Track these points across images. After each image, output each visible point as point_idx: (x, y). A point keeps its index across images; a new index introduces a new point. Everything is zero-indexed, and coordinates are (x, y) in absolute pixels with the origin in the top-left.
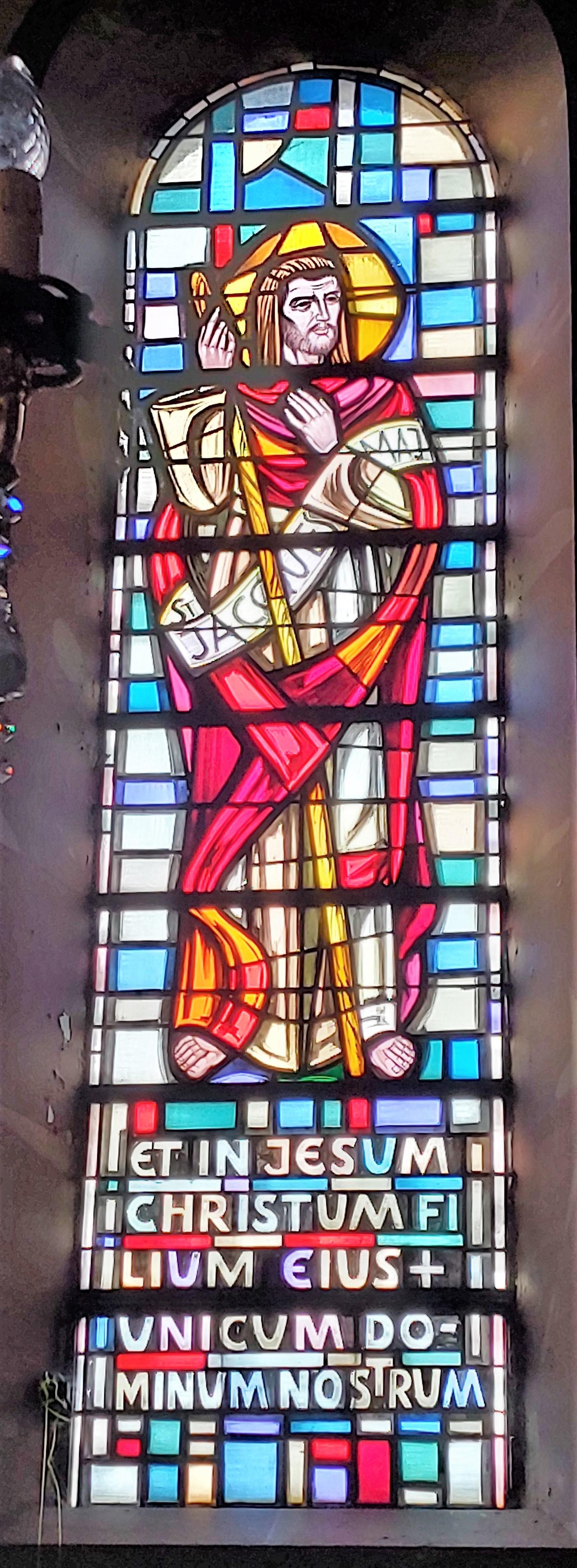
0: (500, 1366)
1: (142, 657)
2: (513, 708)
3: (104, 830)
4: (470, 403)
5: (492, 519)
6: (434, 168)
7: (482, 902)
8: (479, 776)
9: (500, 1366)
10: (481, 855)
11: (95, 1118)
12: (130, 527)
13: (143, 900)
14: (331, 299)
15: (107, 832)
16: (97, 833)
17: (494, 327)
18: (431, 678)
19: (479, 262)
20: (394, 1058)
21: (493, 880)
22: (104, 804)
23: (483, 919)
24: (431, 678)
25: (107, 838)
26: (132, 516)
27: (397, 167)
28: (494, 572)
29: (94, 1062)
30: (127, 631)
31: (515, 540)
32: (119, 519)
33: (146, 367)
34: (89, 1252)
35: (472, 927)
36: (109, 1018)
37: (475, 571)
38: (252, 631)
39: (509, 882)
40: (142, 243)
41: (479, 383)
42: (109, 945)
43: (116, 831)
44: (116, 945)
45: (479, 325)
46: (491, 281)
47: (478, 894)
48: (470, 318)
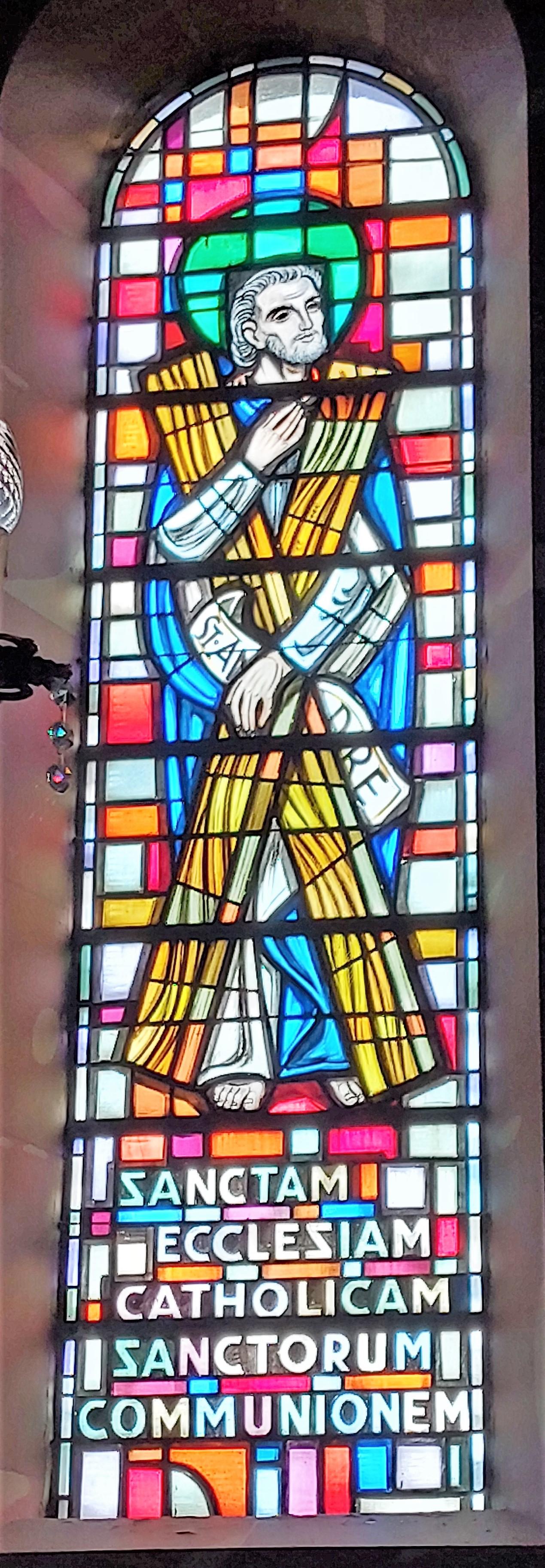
3: (69, 1284)
4: (452, 832)
5: (469, 539)
8: (458, 592)
11: (91, 773)
14: (311, 306)
15: (89, 870)
16: (77, 869)
17: (471, 340)
19: (460, 623)
22: (60, 1494)
25: (88, 877)
29: (69, 1350)
32: (71, 1241)
33: (84, 1515)
34: (92, 845)
36: (106, 611)
37: (455, 591)
41: (461, 939)
43: (98, 868)
48: (448, 511)
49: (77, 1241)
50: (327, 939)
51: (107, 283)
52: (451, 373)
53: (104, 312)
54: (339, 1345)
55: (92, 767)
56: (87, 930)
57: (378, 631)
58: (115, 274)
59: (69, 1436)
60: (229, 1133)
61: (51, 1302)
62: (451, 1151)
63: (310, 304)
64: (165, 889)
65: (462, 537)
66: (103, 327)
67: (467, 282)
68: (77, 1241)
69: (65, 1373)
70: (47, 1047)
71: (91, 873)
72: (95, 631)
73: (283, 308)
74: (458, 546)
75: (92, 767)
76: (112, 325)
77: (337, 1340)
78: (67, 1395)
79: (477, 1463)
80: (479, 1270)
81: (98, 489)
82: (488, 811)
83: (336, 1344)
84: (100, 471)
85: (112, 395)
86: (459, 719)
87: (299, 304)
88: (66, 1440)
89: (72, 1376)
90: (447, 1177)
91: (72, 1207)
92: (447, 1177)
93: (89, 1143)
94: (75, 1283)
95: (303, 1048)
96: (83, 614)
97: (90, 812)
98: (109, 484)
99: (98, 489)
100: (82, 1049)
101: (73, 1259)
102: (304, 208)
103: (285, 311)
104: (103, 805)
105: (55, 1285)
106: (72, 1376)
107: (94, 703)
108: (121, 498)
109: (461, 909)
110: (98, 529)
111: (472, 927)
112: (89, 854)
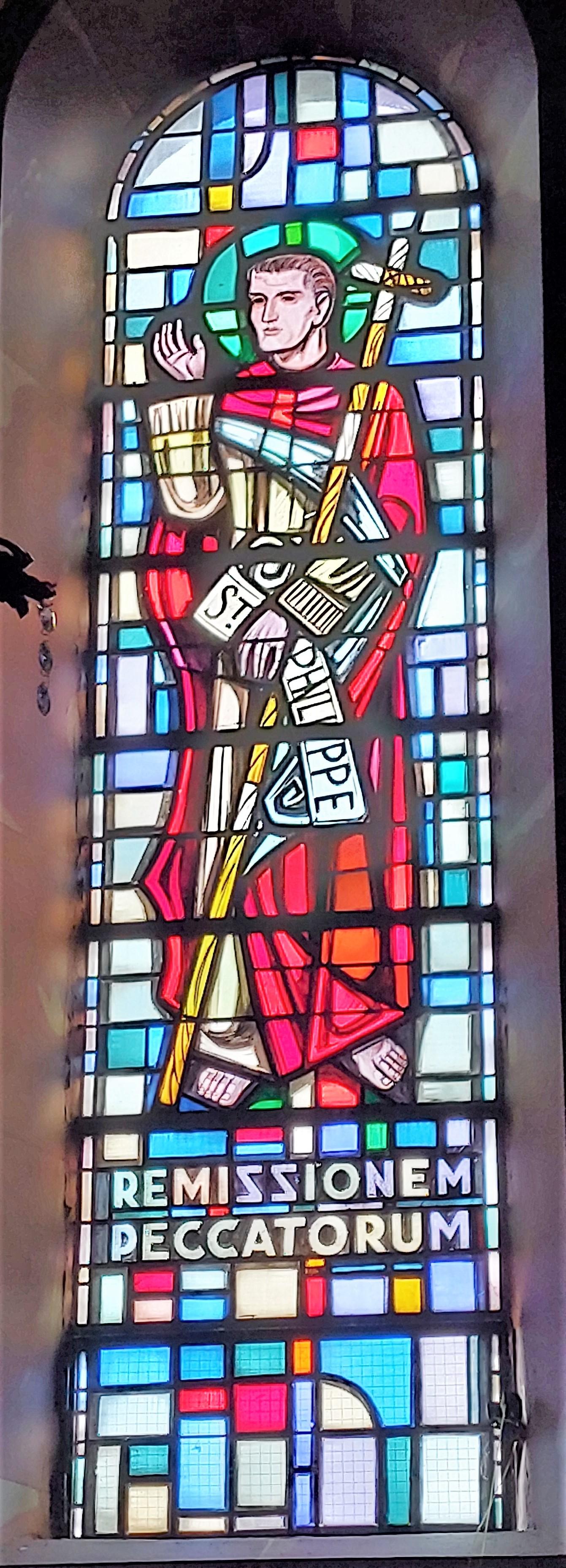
0: (467, 154)
1: (134, 501)
2: (498, 616)
6: (413, 166)
7: (474, 922)
9: (467, 154)
10: (474, 973)
12: (116, 541)
13: (130, 930)
18: (425, 976)
20: (391, 1062)
21: (486, 899)
23: (471, 742)
24: (425, 976)
26: (117, 525)
27: (375, 166)
28: (494, 1078)
30: (119, 481)
31: (517, 1116)
35: (462, 751)
38: (238, 540)
39: (502, 903)
40: (122, 285)
41: (471, 742)
42: (103, 888)
44: (111, 791)
45: (456, 159)
46: (479, 451)
47: (469, 913)
51: (105, 628)
52: (468, 718)
53: (102, 645)
56: (88, 1118)
59: (83, 1227)
61: (83, 541)
62: (461, 653)
65: (467, 184)
70: (64, 771)
72: (88, 1153)
74: (463, 192)
76: (100, 1079)
79: (487, 946)
80: (496, 1202)
82: (502, 855)
84: (108, 460)
86: (462, 186)
90: (454, 678)
92: (454, 678)
93: (114, 580)
100: (101, 714)
104: (103, 1029)
105: (89, 449)
108: (124, 663)
109: (482, 1308)
110: (96, 883)
111: (483, 728)
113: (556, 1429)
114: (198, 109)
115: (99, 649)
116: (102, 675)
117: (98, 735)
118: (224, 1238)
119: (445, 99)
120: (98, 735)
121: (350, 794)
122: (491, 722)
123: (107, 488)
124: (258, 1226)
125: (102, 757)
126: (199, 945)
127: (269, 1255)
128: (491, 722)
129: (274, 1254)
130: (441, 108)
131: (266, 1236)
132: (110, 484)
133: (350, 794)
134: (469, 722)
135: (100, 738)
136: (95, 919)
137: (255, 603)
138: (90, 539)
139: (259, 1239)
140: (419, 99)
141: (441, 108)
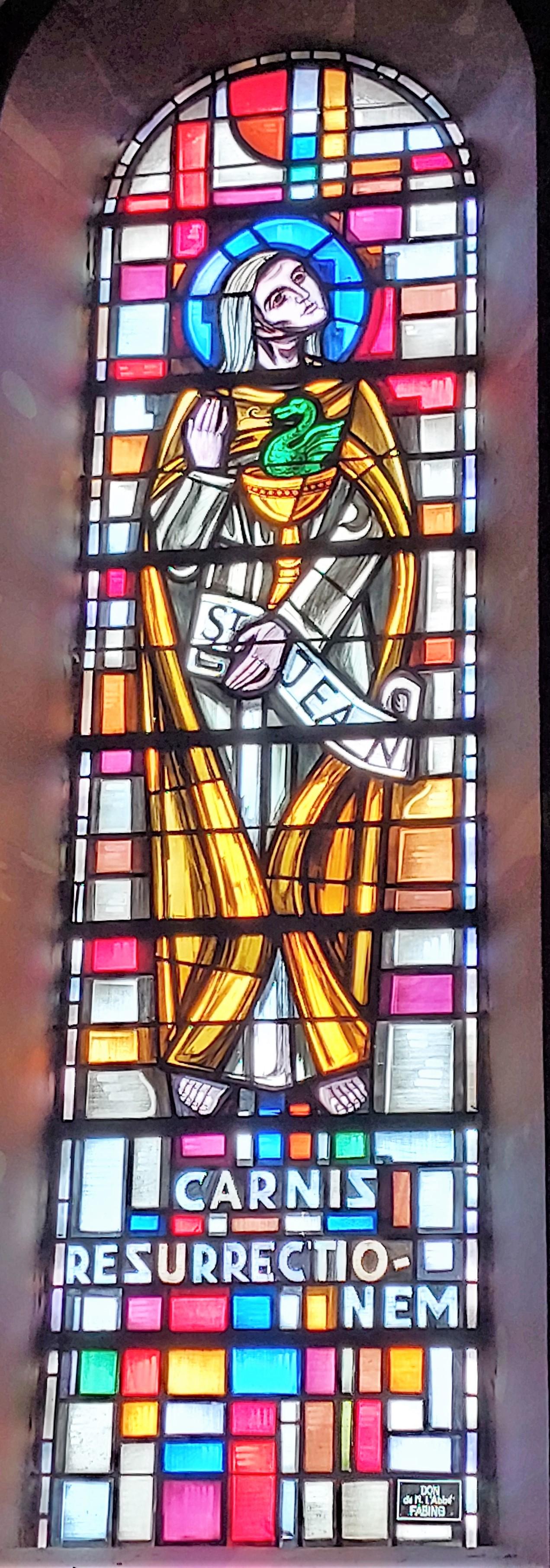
11: (107, 241)
49: (78, 979)
50: (285, 937)
54: (265, 1184)
55: (107, 233)
57: (358, 682)
58: (112, 356)
60: (182, 936)
63: (298, 279)
64: (149, 968)
66: (96, 484)
67: (472, 269)
68: (78, 979)
69: (93, 495)
71: (98, 502)
73: (277, 290)
75: (107, 233)
77: (263, 1177)
78: (89, 650)
81: (101, 360)
83: (261, 1182)
85: (104, 555)
87: (289, 283)
88: (104, 305)
89: (67, 1201)
91: (80, 814)
94: (77, 999)
95: (191, 501)
96: (44, 1322)
97: (88, 677)
98: (108, 431)
99: (101, 360)
101: (97, 457)
102: (287, 156)
103: (277, 294)
106: (67, 1201)
107: (84, 798)
112: (93, 588)
113: (529, 1563)
114: (205, 350)
115: (73, 972)
116: (74, 995)
117: (65, 1118)
118: (192, 1189)
119: (482, 343)
120: (65, 1118)
121: (325, 681)
122: (476, 726)
123: (99, 441)
124: (226, 1177)
125: (69, 1142)
126: (176, 402)
127: (234, 1208)
128: (476, 726)
129: (240, 1207)
130: (447, 115)
131: (232, 1188)
132: (104, 363)
133: (325, 681)
134: (456, 727)
135: (67, 1121)
136: (56, 1326)
137: (257, 1277)
138: (47, 1214)
139: (225, 1190)
140: (427, 105)
141: (447, 115)
